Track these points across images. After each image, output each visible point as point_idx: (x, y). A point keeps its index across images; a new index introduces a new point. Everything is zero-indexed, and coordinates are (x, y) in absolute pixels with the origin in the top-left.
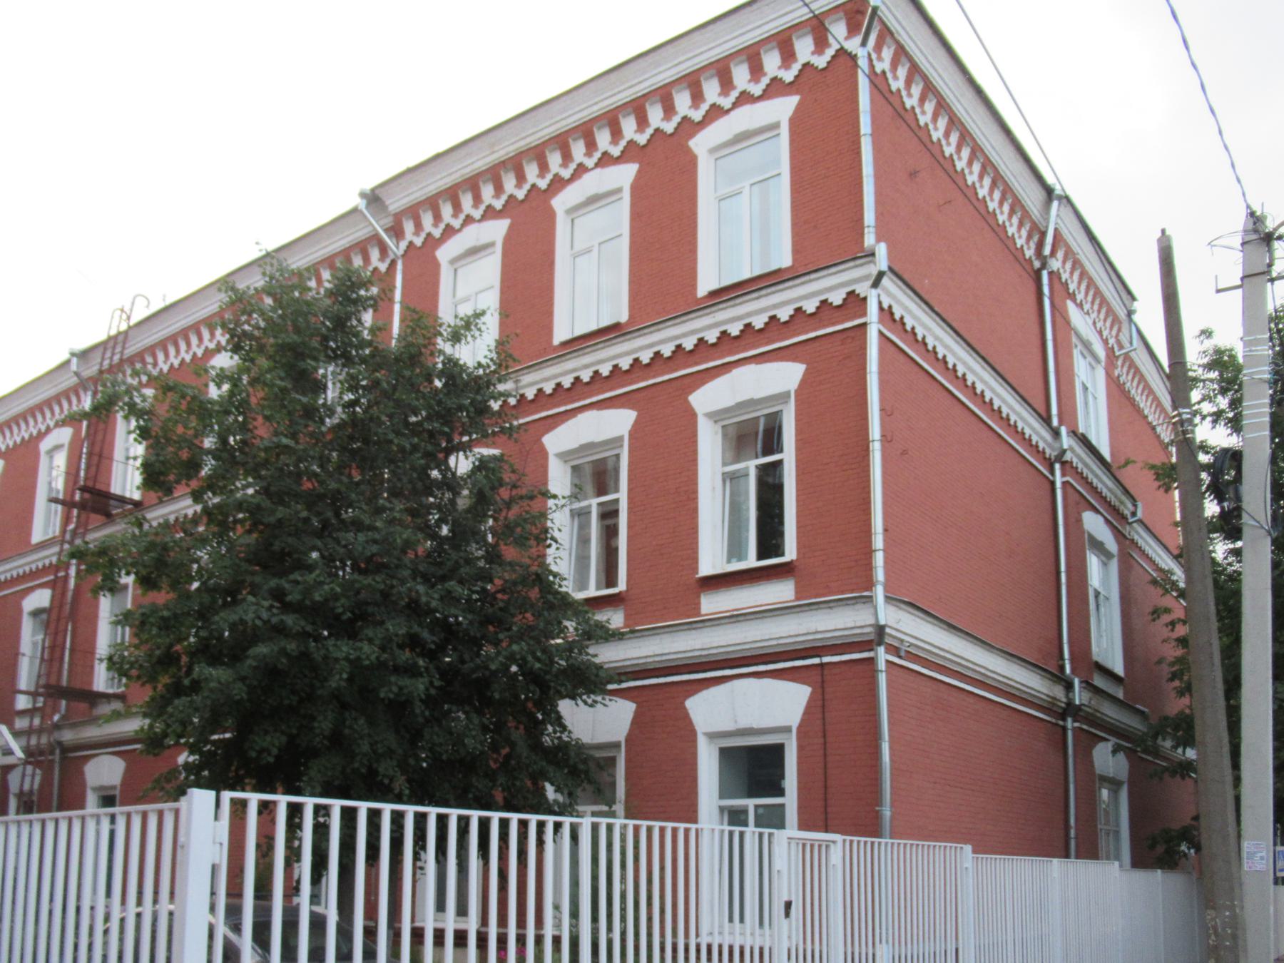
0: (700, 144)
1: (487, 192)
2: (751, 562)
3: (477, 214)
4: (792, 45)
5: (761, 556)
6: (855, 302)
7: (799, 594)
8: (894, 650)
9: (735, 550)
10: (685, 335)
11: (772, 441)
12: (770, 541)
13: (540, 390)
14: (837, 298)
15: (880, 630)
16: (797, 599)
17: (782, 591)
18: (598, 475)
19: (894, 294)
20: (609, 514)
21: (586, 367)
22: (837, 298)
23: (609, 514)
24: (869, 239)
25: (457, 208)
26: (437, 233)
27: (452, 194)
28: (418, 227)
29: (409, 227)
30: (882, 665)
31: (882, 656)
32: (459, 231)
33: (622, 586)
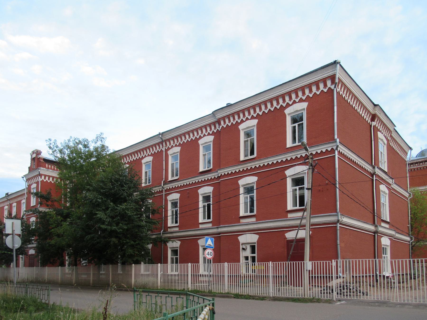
0: (200, 142)
1: (252, 111)
2: (298, 207)
3: (250, 117)
4: (319, 86)
5: (300, 206)
6: (333, 151)
7: (213, 226)
8: (340, 224)
9: (246, 211)
10: (283, 158)
11: (176, 207)
12: (252, 211)
13: (251, 167)
14: (329, 149)
15: (338, 220)
16: (256, 221)
17: (253, 220)
18: (207, 198)
19: (342, 149)
20: (209, 206)
21: (285, 158)
22: (329, 149)
23: (209, 206)
24: (336, 137)
25: (290, 98)
26: (284, 105)
27: (289, 94)
28: (225, 122)
29: (222, 122)
30: (338, 228)
31: (339, 225)
32: (171, 148)
33: (255, 213)
